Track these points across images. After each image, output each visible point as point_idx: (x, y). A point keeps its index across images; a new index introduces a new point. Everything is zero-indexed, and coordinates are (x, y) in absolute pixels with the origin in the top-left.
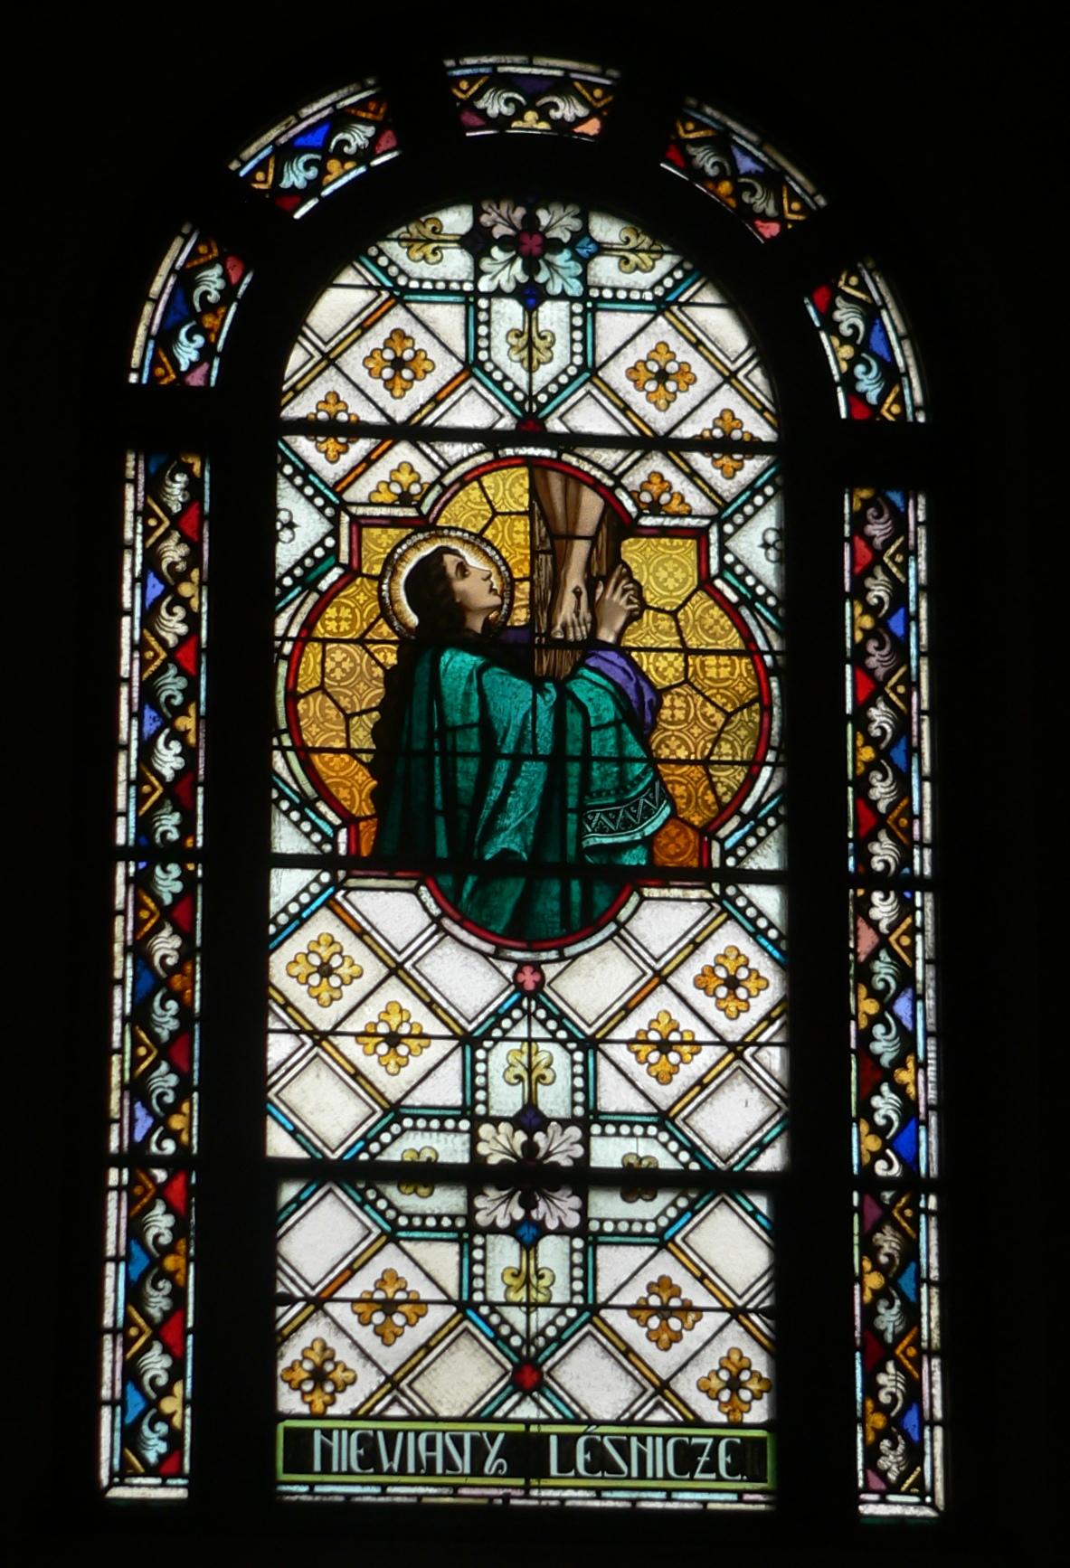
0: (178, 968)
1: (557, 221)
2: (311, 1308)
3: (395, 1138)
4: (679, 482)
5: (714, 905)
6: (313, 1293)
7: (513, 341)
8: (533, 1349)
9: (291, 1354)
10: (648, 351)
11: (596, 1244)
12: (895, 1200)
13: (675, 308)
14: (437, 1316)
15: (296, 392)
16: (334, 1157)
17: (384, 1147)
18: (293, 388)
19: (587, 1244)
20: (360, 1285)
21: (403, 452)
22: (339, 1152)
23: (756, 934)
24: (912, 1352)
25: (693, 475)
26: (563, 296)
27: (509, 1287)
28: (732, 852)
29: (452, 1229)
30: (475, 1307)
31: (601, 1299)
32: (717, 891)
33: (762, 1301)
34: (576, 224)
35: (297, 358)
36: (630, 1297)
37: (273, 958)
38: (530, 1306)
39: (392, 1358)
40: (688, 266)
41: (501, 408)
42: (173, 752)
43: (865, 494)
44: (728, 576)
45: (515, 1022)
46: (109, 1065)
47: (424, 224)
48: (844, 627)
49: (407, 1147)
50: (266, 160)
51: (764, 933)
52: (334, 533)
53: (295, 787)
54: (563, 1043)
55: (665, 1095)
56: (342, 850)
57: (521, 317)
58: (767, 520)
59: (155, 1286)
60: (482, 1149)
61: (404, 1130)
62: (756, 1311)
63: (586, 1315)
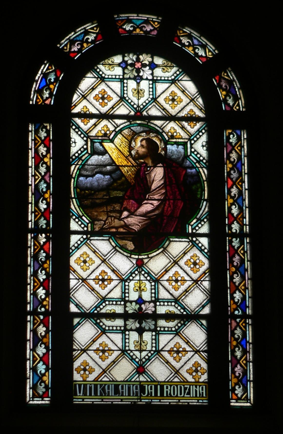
0: (45, 336)
1: (146, 58)
2: (83, 352)
3: (104, 307)
4: (179, 130)
5: (190, 243)
6: (83, 348)
7: (136, 344)
8: (142, 362)
9: (76, 364)
10: (173, 345)
11: (159, 334)
12: (240, 321)
13: (177, 82)
14: (116, 354)
15: (75, 106)
16: (88, 312)
17: (101, 309)
18: (75, 105)
19: (156, 334)
20: (96, 346)
21: (105, 122)
22: (89, 311)
23: (201, 251)
24: (242, 252)
25: (183, 128)
26: (147, 79)
27: (135, 345)
28: (195, 228)
29: (120, 330)
30: (126, 351)
31: (160, 348)
32: (191, 239)
33: (204, 348)
34: (150, 59)
35: (75, 97)
36: (167, 348)
37: (71, 258)
38: (141, 351)
39: (104, 365)
40: (180, 70)
41: (130, 109)
42: (42, 387)
43: (230, 131)
44: (193, 154)
45: (136, 275)
46: (28, 153)
47: (109, 60)
48: (229, 386)
49: (108, 309)
50: (67, 43)
51: (203, 250)
52: (87, 144)
53: (76, 212)
54: (149, 281)
55: (177, 294)
56: (89, 230)
57: (138, 337)
58: (204, 138)
59: (42, 166)
60: (127, 309)
61: (106, 305)
62: (202, 351)
63: (156, 353)
